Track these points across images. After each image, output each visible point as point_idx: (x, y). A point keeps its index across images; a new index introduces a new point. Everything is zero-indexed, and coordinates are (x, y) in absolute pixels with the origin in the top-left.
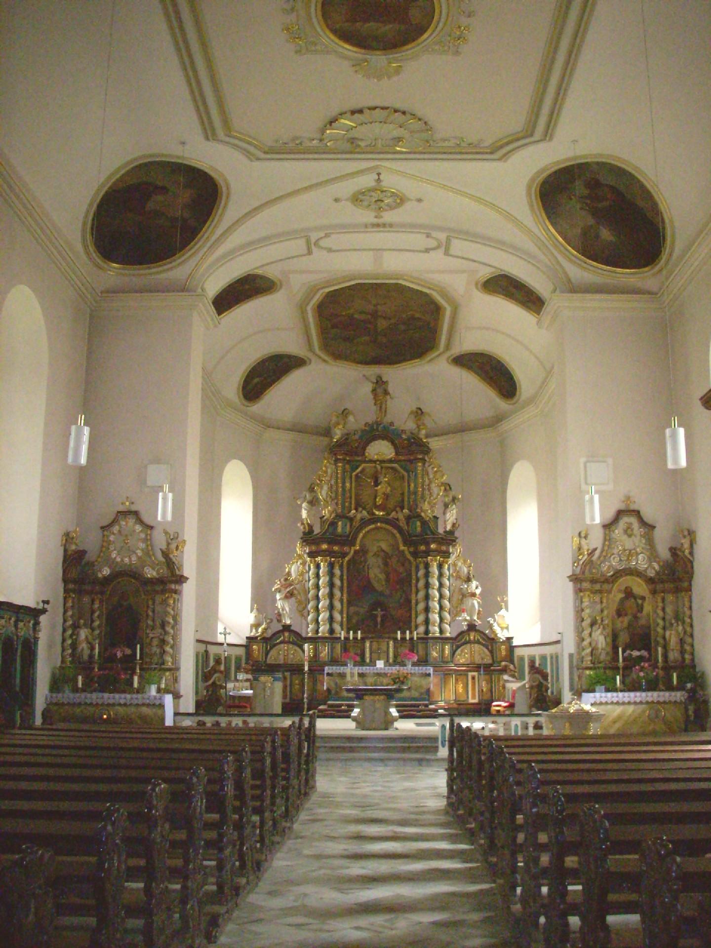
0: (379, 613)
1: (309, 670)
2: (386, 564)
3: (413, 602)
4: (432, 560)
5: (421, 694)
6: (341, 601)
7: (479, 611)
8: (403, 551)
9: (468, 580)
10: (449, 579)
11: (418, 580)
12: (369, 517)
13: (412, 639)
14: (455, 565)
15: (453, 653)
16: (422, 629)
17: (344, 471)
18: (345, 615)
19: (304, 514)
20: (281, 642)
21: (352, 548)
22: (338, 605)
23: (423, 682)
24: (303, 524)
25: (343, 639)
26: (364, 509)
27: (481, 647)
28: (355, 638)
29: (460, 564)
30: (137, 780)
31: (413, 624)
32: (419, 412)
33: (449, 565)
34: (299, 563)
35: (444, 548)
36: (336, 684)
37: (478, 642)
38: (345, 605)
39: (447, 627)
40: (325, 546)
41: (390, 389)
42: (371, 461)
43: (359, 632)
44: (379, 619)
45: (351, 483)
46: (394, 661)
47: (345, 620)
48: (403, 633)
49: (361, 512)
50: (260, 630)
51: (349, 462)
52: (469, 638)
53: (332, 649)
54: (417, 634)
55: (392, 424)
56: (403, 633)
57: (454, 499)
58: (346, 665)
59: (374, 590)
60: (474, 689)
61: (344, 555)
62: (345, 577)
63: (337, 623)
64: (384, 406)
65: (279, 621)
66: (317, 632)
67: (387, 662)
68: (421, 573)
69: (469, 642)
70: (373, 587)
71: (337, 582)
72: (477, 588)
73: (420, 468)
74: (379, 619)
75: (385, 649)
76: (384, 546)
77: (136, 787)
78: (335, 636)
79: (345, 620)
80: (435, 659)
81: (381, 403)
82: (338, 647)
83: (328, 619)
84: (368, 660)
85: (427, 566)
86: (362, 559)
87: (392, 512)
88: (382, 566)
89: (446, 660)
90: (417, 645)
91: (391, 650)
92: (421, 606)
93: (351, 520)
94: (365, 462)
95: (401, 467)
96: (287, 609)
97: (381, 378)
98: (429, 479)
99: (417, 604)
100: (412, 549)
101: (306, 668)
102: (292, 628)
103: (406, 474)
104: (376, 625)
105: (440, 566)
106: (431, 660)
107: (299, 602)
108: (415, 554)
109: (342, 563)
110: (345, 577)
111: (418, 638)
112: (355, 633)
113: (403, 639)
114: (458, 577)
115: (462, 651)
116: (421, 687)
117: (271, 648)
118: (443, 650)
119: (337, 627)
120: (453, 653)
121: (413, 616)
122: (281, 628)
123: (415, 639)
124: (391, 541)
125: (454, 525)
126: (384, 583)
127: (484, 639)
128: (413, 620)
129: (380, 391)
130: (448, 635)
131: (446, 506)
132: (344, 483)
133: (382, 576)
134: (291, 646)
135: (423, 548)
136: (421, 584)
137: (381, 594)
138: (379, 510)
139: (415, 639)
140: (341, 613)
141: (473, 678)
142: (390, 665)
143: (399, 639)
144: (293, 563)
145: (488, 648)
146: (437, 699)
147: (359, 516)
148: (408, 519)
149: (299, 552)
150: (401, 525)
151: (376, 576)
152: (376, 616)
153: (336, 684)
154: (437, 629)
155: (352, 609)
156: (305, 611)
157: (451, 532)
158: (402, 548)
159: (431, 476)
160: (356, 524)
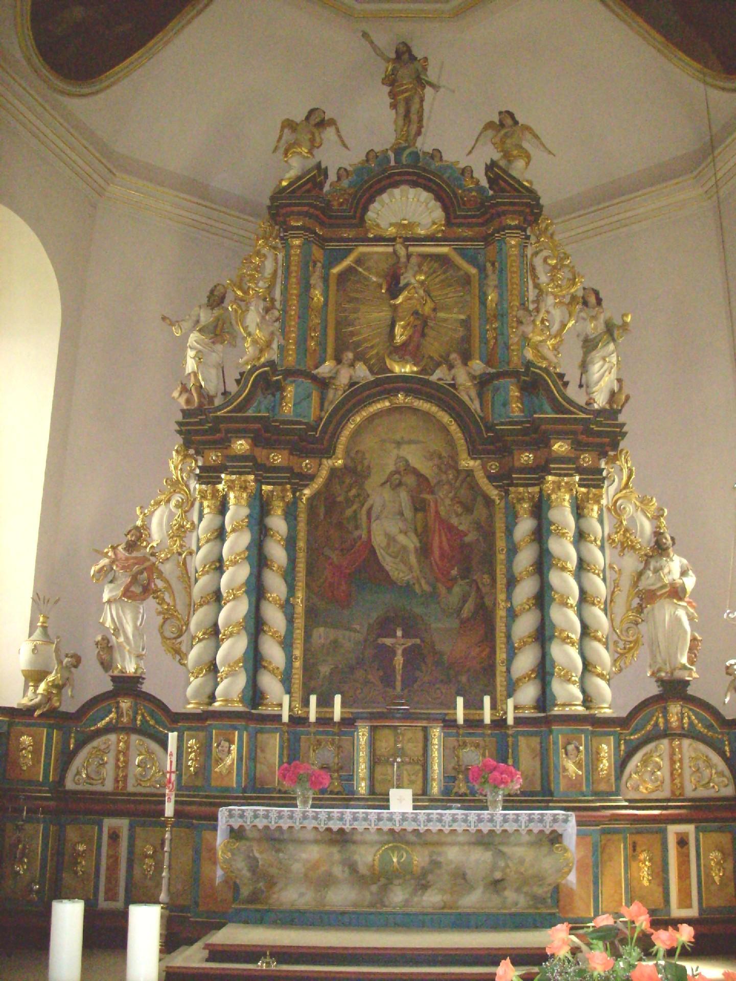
0: (398, 642)
1: (177, 813)
2: (419, 506)
3: (501, 613)
4: (558, 486)
5: (537, 900)
6: (287, 607)
7: (694, 639)
8: (469, 473)
9: (659, 548)
10: (602, 548)
11: (513, 550)
12: (372, 378)
13: (499, 723)
14: (616, 510)
15: (621, 765)
16: (528, 693)
17: (307, 264)
18: (298, 652)
19: (191, 365)
20: (108, 729)
21: (325, 461)
22: (275, 618)
23: (547, 863)
24: (185, 389)
25: (285, 719)
26: (359, 357)
27: (702, 747)
28: (324, 721)
29: (630, 509)
30: (211, 804)
31: (500, 680)
32: (509, 121)
33: (600, 509)
34: (173, 503)
35: (586, 459)
36: (254, 866)
37: (692, 734)
38: (299, 623)
39: (602, 684)
40: (241, 445)
41: (432, 74)
42: (379, 239)
43: (338, 699)
44: (399, 660)
45: (326, 293)
46: (446, 791)
47: (297, 664)
48: (474, 704)
49: (352, 365)
50: (42, 687)
51: (322, 241)
52: (667, 722)
53: (252, 755)
54: (516, 708)
55: (436, 154)
56: (474, 704)
57: (610, 330)
58: (290, 801)
59: (381, 578)
60: (684, 875)
61: (307, 478)
62: (301, 544)
63: (272, 672)
64: (415, 107)
65: (107, 665)
66: (212, 698)
67: (422, 798)
68: (525, 526)
69: (666, 733)
70: (381, 569)
71: (277, 553)
72: (684, 573)
73: (514, 251)
74: (399, 660)
75: (414, 749)
76: (416, 458)
77: (208, 809)
78: (262, 710)
79: (297, 664)
80: (574, 784)
81: (408, 101)
82: (273, 744)
83: (245, 658)
84: (362, 788)
85: (540, 509)
86: (353, 492)
87: (438, 365)
88: (408, 513)
89: (603, 787)
90: (516, 745)
91: (436, 754)
92: (525, 625)
93: (324, 384)
94: (365, 240)
95: (462, 253)
96: (129, 629)
97: (409, 50)
98: (536, 286)
99: (512, 614)
100: (494, 467)
101: (169, 809)
102: (146, 687)
103: (473, 271)
104: (388, 680)
105: (579, 511)
106: (561, 787)
107: (168, 615)
108: (503, 480)
109: (296, 501)
110: (301, 544)
111: (518, 721)
112: (325, 702)
113: (474, 723)
114: (626, 546)
115: (645, 761)
116: (539, 879)
117: (80, 746)
118: (593, 758)
119: (271, 685)
120: (621, 765)
121: (501, 655)
122: (109, 686)
123: (510, 721)
124: (437, 444)
125: (613, 395)
126: (413, 559)
127: (710, 727)
128: (501, 669)
129: (405, 75)
130: (606, 711)
131: (589, 345)
132: (306, 288)
133: (410, 542)
134: (135, 739)
135: (527, 457)
136: (525, 558)
137: (407, 589)
138: (403, 360)
139: (510, 721)
140: (287, 644)
141: (682, 842)
142: (434, 803)
143: (460, 720)
144: (158, 504)
145: (722, 754)
146: (583, 914)
147: (344, 378)
148: (483, 383)
149: (175, 475)
150: (465, 398)
151: (391, 539)
152: (391, 652)
153: (254, 866)
154: (575, 691)
155: (321, 634)
156: (184, 638)
157: (611, 412)
158: (467, 463)
159: (543, 279)
160: (335, 396)
